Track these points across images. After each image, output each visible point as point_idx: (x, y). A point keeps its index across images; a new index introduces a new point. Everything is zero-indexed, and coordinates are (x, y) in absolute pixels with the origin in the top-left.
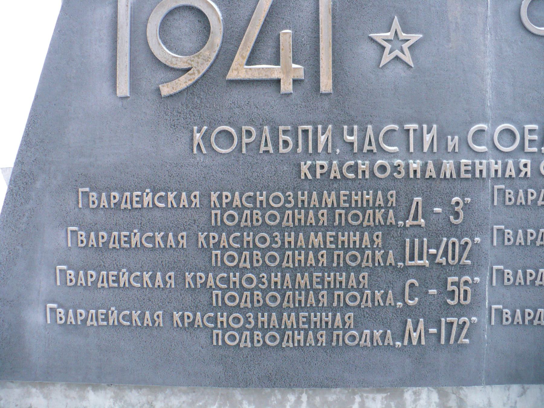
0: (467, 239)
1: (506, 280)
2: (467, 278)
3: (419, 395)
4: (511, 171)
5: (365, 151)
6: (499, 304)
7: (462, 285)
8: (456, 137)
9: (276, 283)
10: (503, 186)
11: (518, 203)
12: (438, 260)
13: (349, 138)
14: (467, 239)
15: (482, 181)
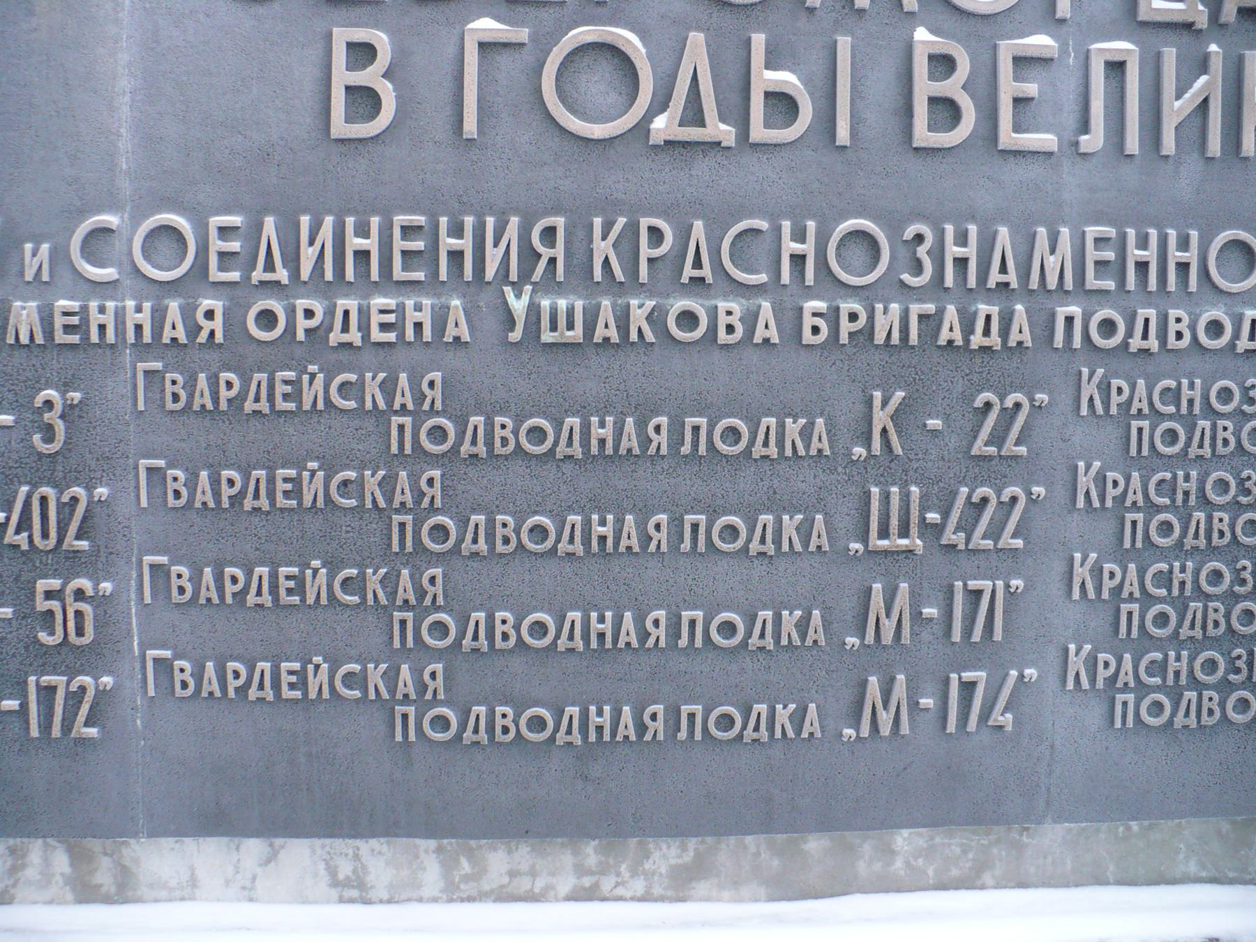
0: (78, 491)
1: (175, 592)
2: (85, 583)
3: (24, 856)
4: (174, 328)
5: (991, 284)
6: (163, 646)
7: (69, 600)
8: (45, 247)
10: (158, 365)
11: (196, 407)
12: (951, 536)
14: (1016, 490)
15: (108, 353)
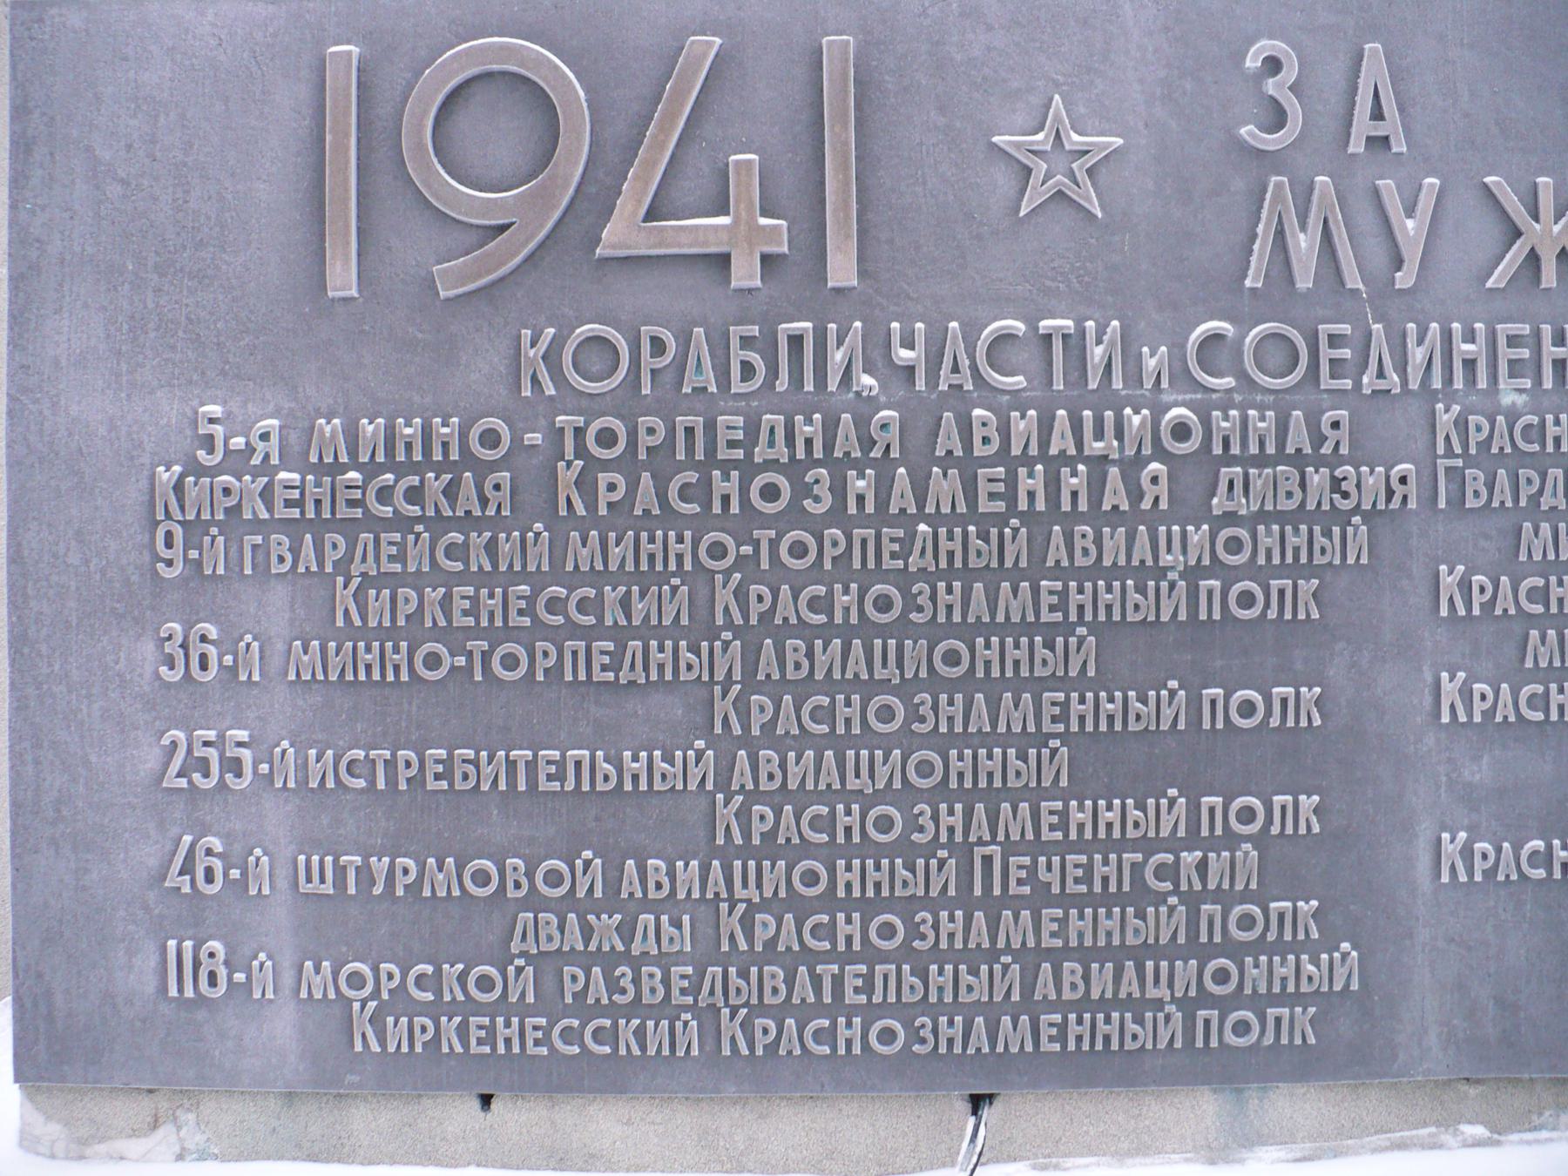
9: (951, 830)
13: (905, 355)
